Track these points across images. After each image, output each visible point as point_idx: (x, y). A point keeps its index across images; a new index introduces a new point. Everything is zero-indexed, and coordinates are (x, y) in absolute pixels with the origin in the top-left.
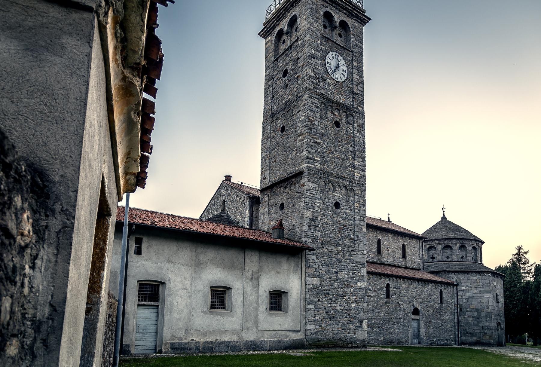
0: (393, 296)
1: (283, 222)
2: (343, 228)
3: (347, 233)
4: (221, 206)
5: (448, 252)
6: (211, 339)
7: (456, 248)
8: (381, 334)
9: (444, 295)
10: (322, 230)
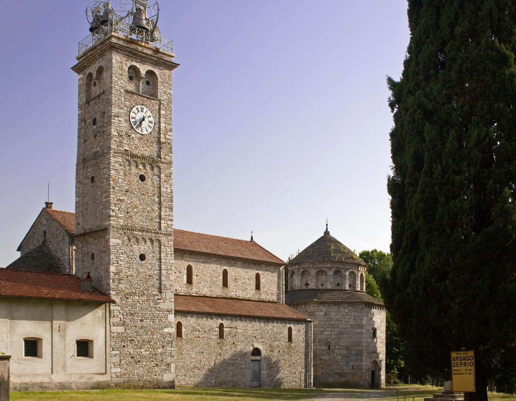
0: (227, 337)
2: (149, 278)
3: (153, 283)
4: (42, 237)
5: (323, 278)
6: (27, 380)
7: (330, 273)
8: (212, 376)
9: (294, 333)
10: (127, 282)
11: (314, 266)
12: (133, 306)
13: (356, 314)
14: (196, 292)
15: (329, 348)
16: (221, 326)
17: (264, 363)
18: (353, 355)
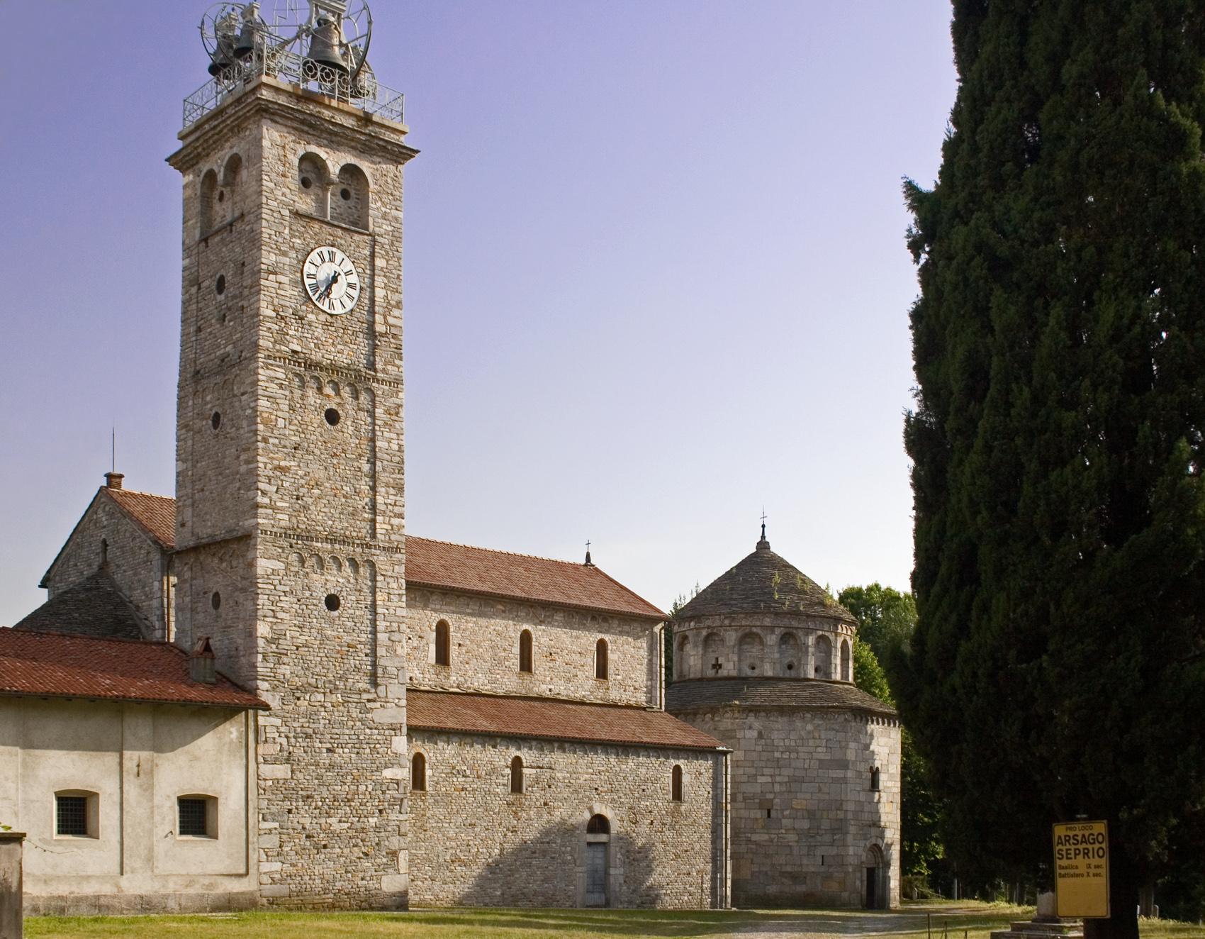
0: (530, 789)
1: (211, 642)
2: (348, 651)
3: (358, 662)
4: (98, 554)
5: (754, 650)
6: (63, 890)
7: (772, 639)
8: (495, 881)
9: (686, 779)
10: (296, 660)
11: (733, 624)
12: (311, 716)
13: (831, 735)
14: (458, 684)
15: (769, 816)
16: (517, 764)
17: (617, 849)
18: (824, 832)
